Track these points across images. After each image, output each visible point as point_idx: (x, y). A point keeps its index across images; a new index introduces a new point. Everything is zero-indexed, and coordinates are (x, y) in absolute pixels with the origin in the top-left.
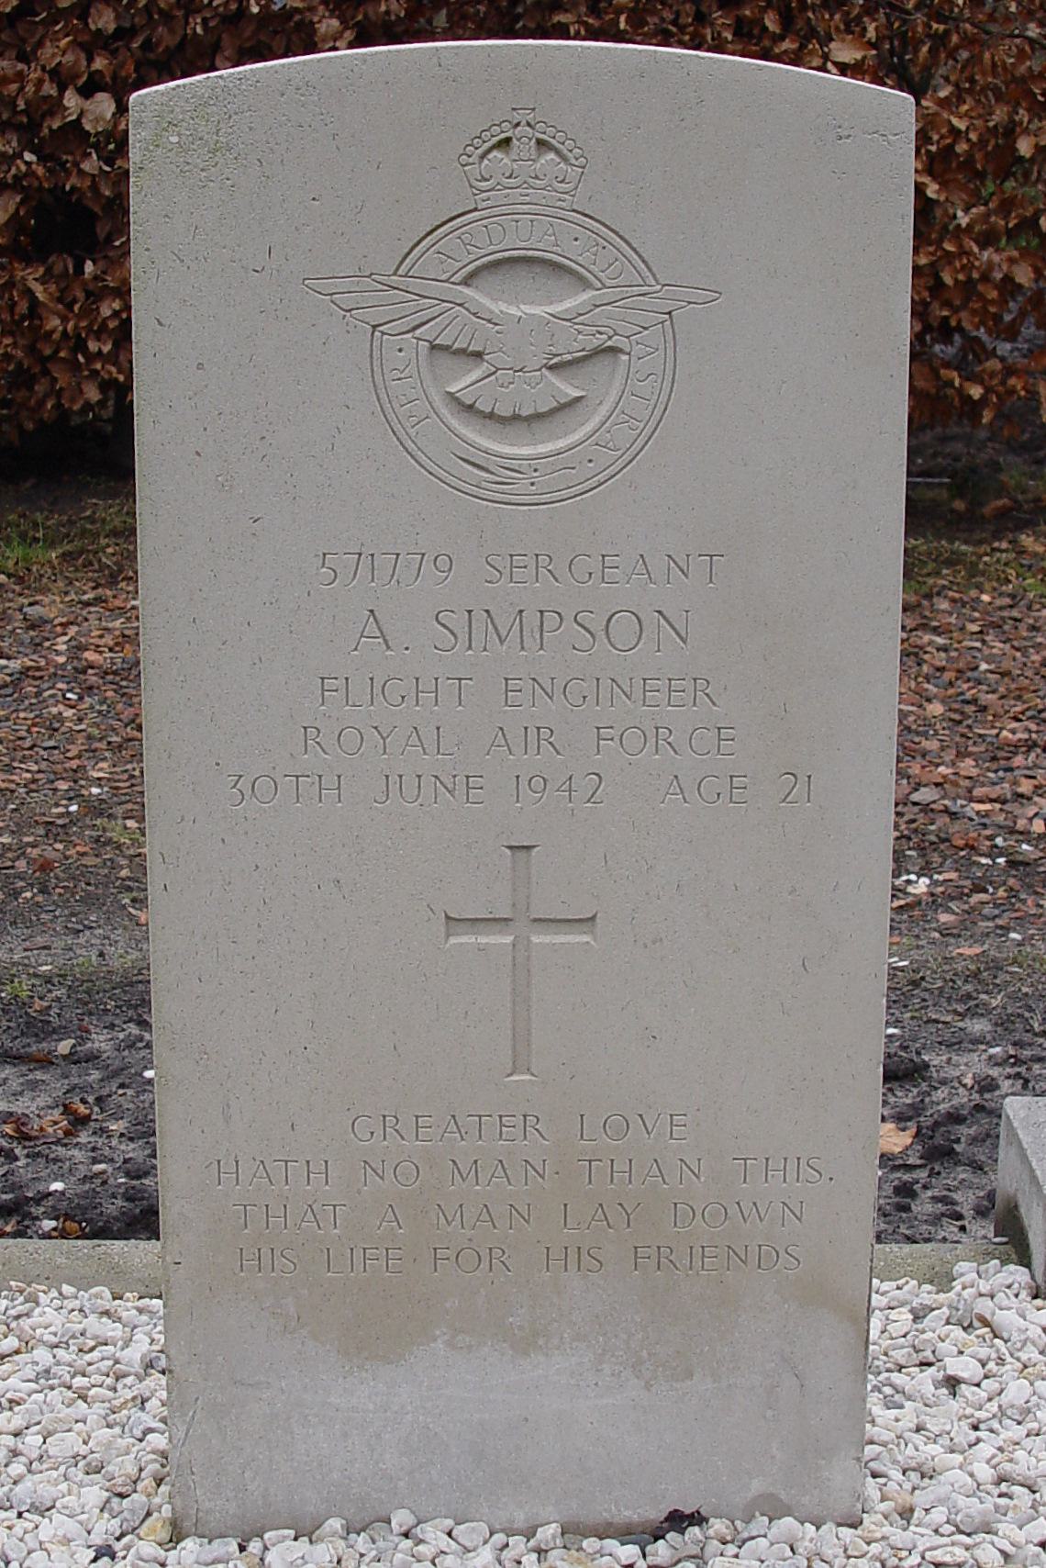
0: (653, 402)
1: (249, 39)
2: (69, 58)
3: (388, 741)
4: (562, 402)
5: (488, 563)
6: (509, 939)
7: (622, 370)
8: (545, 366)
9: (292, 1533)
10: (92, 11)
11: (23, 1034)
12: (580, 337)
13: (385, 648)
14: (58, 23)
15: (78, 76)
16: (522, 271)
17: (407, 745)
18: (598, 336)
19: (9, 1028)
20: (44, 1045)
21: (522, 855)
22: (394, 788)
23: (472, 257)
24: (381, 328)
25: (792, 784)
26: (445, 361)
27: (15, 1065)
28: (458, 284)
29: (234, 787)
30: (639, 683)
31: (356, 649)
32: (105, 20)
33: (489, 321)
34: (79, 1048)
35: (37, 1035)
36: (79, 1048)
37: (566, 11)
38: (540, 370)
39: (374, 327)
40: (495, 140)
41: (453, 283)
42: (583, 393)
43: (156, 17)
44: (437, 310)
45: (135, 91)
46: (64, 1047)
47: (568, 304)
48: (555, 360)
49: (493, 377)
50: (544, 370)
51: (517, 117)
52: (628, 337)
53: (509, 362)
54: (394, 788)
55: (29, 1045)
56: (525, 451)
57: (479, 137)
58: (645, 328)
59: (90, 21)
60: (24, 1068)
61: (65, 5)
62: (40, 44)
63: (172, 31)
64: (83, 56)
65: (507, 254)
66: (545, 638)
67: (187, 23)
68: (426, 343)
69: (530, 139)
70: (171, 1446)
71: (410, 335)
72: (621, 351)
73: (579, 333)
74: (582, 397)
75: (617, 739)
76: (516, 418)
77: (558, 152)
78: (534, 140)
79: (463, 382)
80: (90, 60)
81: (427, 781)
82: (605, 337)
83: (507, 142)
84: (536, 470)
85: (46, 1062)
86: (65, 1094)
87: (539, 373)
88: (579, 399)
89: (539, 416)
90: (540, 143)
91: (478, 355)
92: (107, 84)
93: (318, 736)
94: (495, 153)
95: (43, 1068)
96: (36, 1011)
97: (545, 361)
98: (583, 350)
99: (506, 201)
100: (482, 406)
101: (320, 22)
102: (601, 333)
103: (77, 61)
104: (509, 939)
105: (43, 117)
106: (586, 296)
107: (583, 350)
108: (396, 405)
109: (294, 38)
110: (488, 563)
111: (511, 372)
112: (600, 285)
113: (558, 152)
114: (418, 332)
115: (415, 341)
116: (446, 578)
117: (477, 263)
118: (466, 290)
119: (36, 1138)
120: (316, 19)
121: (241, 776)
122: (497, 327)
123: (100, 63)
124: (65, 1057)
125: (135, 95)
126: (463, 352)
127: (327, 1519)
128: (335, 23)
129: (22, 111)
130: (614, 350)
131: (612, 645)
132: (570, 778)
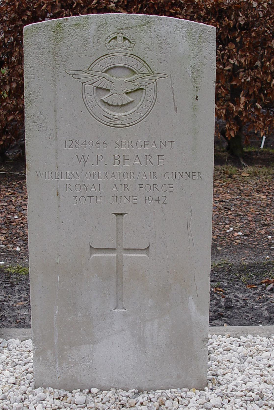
0: (151, 102)
3: (87, 188)
4: (129, 101)
5: (116, 143)
6: (115, 255)
7: (144, 93)
8: (125, 93)
9: (79, 390)
12: (133, 86)
13: (140, 164)
16: (119, 69)
17: (113, 189)
18: (138, 86)
21: (120, 217)
23: (107, 66)
24: (85, 83)
26: (99, 91)
28: (103, 73)
29: (75, 199)
30: (191, 173)
31: (133, 165)
33: (111, 82)
38: (123, 94)
39: (83, 83)
40: (113, 37)
41: (102, 72)
42: (133, 100)
44: (99, 79)
45: (25, 26)
47: (131, 78)
48: (127, 92)
49: (112, 96)
50: (125, 94)
51: (118, 31)
52: (145, 86)
53: (116, 92)
56: (120, 114)
57: (109, 36)
58: (150, 84)
65: (115, 65)
66: (98, 162)
68: (95, 87)
69: (122, 37)
71: (91, 85)
72: (144, 89)
73: (133, 85)
74: (134, 101)
75: (144, 187)
76: (118, 105)
77: (128, 40)
78: (122, 37)
79: (105, 97)
81: (123, 198)
82: (139, 86)
83: (116, 38)
84: (122, 119)
87: (123, 95)
88: (132, 102)
89: (112, 105)
90: (124, 38)
91: (109, 90)
93: (127, 187)
94: (113, 40)
97: (125, 92)
98: (134, 89)
99: (120, 52)
100: (109, 103)
102: (139, 85)
104: (115, 255)
107: (134, 89)
108: (88, 102)
110: (116, 143)
111: (116, 94)
112: (138, 73)
113: (128, 40)
114: (93, 84)
115: (93, 87)
116: (92, 147)
117: (133, 68)
118: (106, 74)
121: (76, 197)
122: (113, 84)
125: (25, 27)
126: (104, 89)
127: (92, 388)
129: (237, 38)
130: (142, 89)
132: (159, 197)
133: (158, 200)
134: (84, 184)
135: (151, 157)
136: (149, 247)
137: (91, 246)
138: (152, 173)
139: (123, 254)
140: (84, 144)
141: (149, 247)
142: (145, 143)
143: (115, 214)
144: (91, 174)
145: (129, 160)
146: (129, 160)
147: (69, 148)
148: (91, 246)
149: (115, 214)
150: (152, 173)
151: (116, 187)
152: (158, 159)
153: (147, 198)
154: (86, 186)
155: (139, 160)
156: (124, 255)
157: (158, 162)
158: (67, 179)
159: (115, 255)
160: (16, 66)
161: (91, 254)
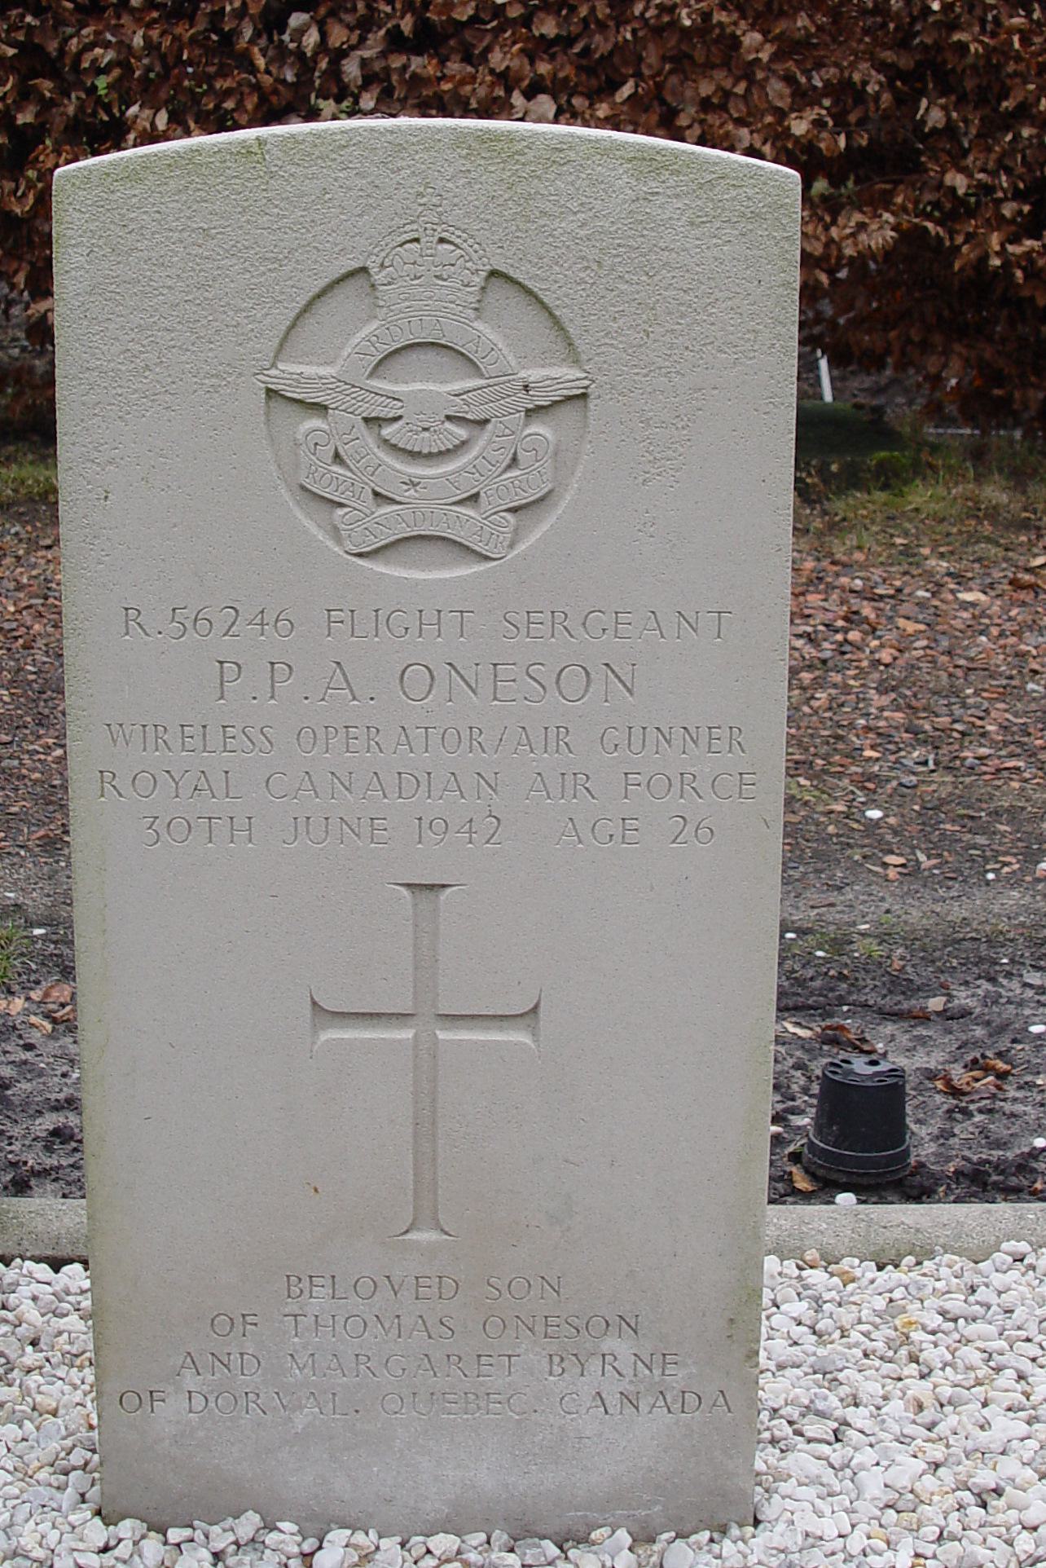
1: (671, 49)
2: (515, 64)
10: (535, 19)
11: (891, 992)
14: (505, 32)
15: (522, 79)
19: (876, 986)
20: (913, 1002)
22: (302, 829)
25: (681, 826)
27: (894, 1022)
32: (548, 27)
34: (950, 1005)
35: (903, 993)
36: (950, 1005)
37: (963, 30)
43: (593, 26)
46: (936, 1003)
54: (302, 829)
55: (900, 1002)
59: (534, 28)
60: (906, 1025)
61: (514, 15)
62: (488, 49)
63: (606, 40)
64: (526, 61)
67: (618, 32)
70: (333, 1526)
80: (532, 63)
85: (924, 1018)
86: (958, 1048)
92: (547, 87)
95: (923, 1023)
96: (896, 970)
101: (744, 34)
103: (522, 66)
105: (768, 102)
106: (483, 382)
109: (713, 49)
119: (964, 1094)
120: (739, 33)
123: (544, 68)
124: (938, 1013)
128: (758, 36)
131: (405, 693)
133: (470, 832)
134: (168, 772)
135: (289, 666)
136: (535, 1009)
137: (314, 1003)
138: (552, 732)
139: (438, 1032)
140: (258, 620)
141: (535, 1009)
142: (532, 620)
143: (408, 886)
144: (318, 736)
145: (514, 681)
146: (514, 681)
147: (226, 638)
148: (314, 1003)
149: (408, 886)
150: (552, 732)
151: (311, 782)
152: (496, 676)
153: (425, 825)
154: (174, 780)
155: (347, 681)
156: (442, 1035)
157: (495, 689)
158: (184, 753)
159: (407, 1034)
160: (964, 243)
161: (315, 1029)
